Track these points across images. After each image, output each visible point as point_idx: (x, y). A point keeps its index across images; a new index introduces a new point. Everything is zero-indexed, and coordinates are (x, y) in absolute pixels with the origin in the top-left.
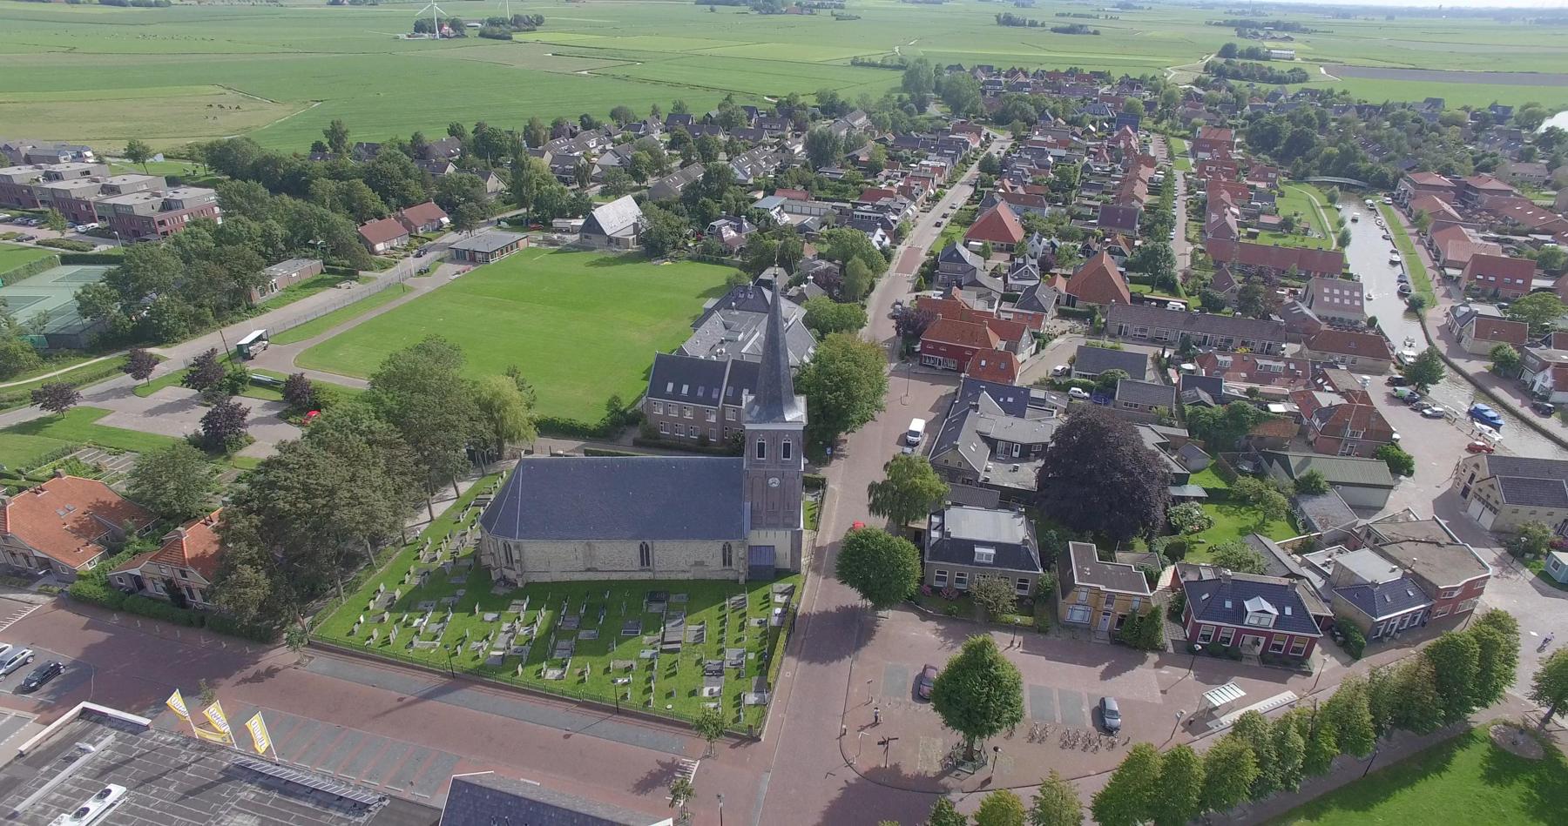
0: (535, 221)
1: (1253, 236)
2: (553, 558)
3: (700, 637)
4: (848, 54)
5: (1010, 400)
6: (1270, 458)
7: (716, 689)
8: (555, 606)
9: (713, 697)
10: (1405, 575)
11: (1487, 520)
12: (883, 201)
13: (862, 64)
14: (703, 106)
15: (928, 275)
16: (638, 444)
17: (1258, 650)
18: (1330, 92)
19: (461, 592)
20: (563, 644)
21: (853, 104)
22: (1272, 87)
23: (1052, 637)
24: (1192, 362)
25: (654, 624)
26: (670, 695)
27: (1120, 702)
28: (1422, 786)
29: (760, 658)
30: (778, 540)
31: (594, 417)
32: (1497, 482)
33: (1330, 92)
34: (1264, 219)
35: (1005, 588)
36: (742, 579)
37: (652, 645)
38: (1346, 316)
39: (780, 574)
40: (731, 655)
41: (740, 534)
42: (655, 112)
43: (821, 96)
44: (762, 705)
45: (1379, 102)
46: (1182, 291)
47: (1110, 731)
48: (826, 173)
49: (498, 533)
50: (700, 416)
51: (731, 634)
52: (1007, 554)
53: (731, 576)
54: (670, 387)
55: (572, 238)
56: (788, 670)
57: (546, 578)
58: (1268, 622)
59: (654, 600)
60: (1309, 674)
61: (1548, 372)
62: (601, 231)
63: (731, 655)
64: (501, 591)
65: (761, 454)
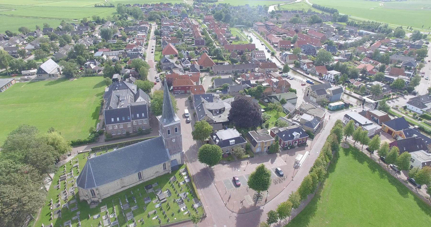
0: (12, 73)
1: (231, 42)
2: (109, 189)
3: (170, 193)
4: (93, 3)
5: (208, 98)
6: (271, 97)
7: (185, 207)
8: (117, 203)
9: (185, 211)
10: (315, 117)
11: (315, 100)
12: (135, 48)
13: (99, 6)
14: (55, 25)
15: (159, 68)
16: (106, 141)
17: (296, 144)
18: (226, 4)
19: (78, 213)
20: (128, 214)
21: (106, 20)
22: (212, 4)
23: (255, 158)
24: (239, 77)
25: (153, 196)
26: (173, 215)
27: (280, 167)
28: (338, 161)
29: (191, 193)
30: (177, 157)
31: (86, 136)
32: (315, 91)
33: (226, 4)
34: (231, 38)
35: (240, 149)
36: (170, 172)
37: (157, 203)
38: (263, 59)
39: (180, 166)
40: (182, 195)
41: (168, 159)
42: (37, 28)
43: (94, 18)
44: (201, 206)
45: (237, 6)
46: (225, 59)
47: (282, 176)
48: (111, 41)
49: (88, 187)
50: (125, 126)
51: (178, 190)
52: (237, 140)
53: (166, 172)
54: (113, 120)
55: (33, 77)
56: (200, 192)
57: (109, 195)
58: (298, 137)
59: (148, 189)
60: (308, 146)
61: (306, 65)
62: (45, 73)
63: (182, 195)
64: (94, 206)
65: (169, 133)
